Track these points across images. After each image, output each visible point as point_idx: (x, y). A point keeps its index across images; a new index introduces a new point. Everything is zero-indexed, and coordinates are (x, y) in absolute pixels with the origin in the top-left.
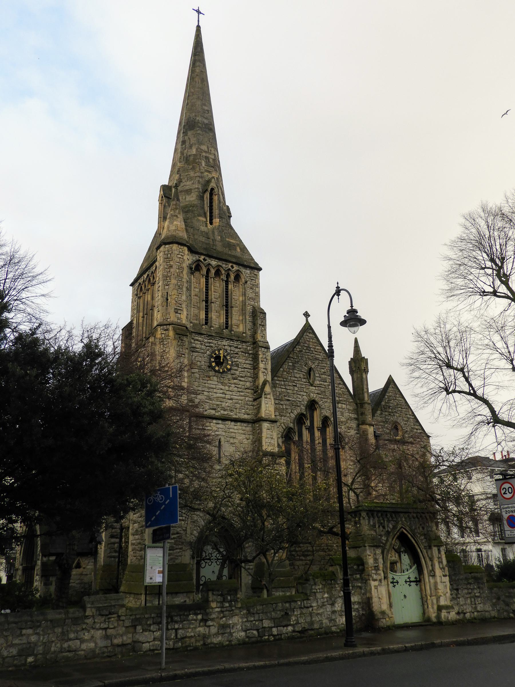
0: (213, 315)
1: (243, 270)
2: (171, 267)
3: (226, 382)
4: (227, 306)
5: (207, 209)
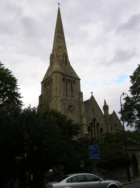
0: (68, 93)
1: (76, 80)
2: (57, 79)
3: (73, 113)
4: (72, 91)
5: (65, 61)
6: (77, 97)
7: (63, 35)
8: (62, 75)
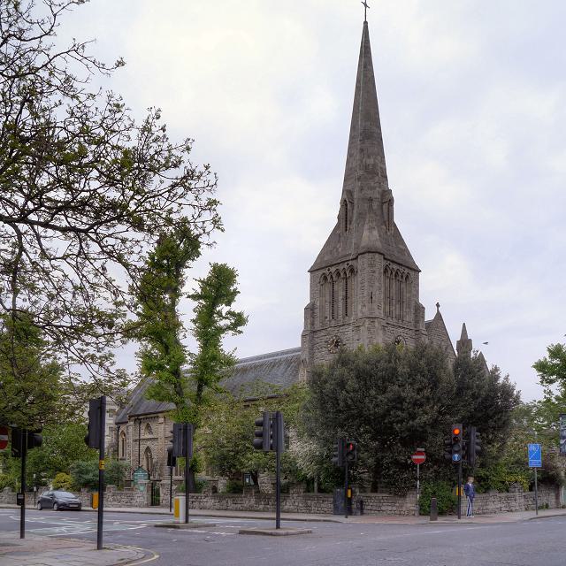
2: (374, 272)
6: (409, 317)
7: (377, 130)
8: (385, 259)
